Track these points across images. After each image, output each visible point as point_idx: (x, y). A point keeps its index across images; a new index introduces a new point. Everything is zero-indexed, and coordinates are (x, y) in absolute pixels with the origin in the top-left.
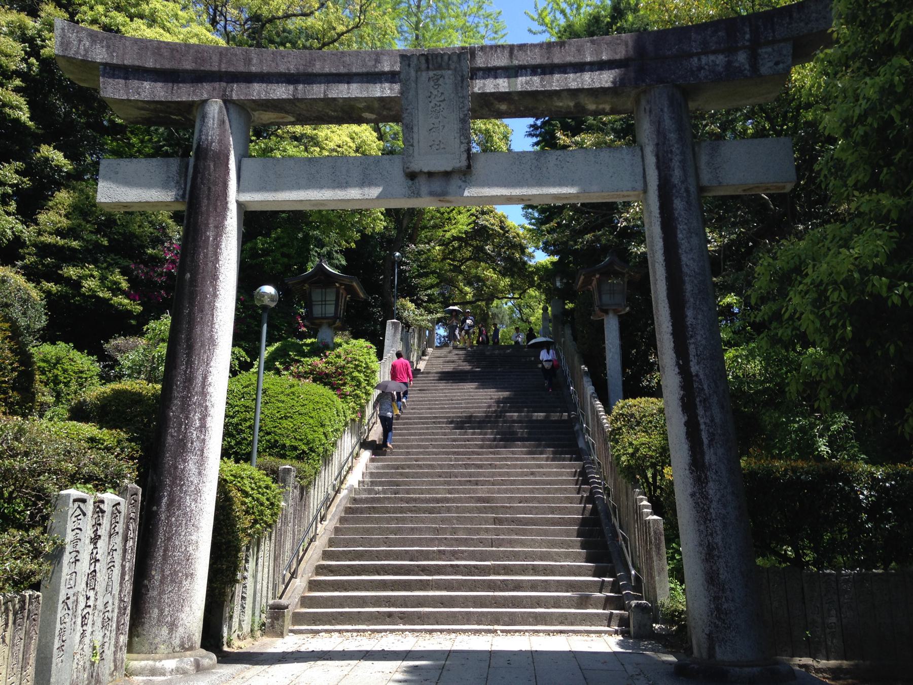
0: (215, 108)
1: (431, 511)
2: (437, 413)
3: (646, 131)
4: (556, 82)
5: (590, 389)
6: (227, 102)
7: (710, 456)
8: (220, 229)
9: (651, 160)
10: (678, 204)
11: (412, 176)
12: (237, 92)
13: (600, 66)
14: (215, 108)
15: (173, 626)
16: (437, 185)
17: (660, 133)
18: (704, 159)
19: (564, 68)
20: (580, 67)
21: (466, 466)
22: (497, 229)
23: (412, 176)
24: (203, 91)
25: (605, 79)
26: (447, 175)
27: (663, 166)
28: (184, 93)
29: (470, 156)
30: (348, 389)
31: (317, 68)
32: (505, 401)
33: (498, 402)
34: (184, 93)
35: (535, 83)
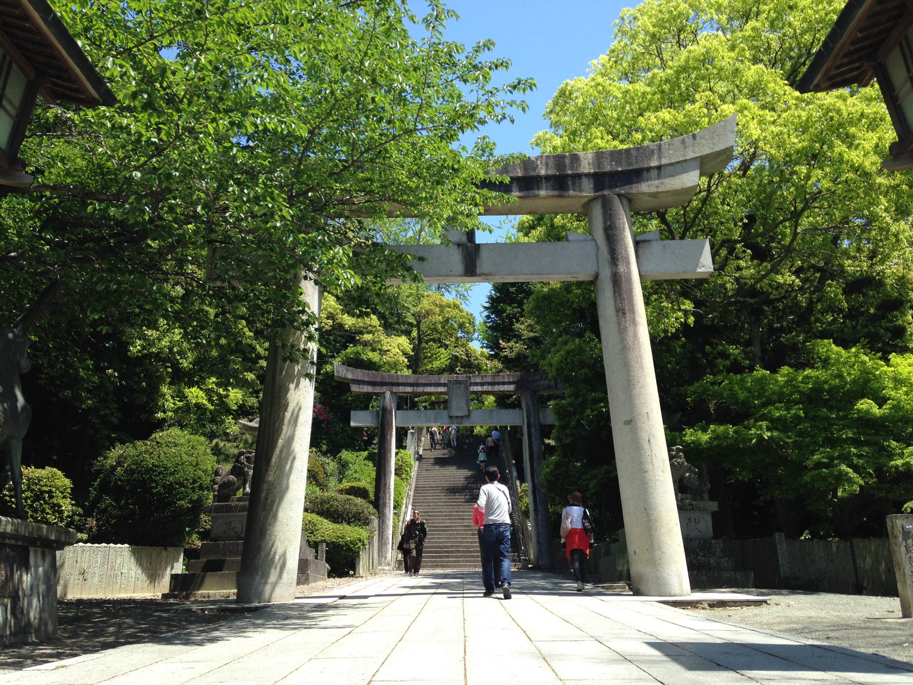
0: (388, 394)
1: (445, 531)
2: (438, 484)
3: (524, 405)
4: (497, 388)
5: (515, 474)
6: (392, 392)
7: (539, 508)
8: (391, 435)
9: (525, 415)
10: (533, 430)
11: (451, 417)
12: (395, 389)
13: (510, 383)
14: (388, 394)
15: (386, 558)
16: (459, 420)
17: (528, 406)
18: (541, 414)
19: (498, 383)
20: (504, 383)
21: (457, 512)
22: (464, 357)
23: (451, 417)
24: (384, 389)
25: (511, 388)
26: (462, 417)
27: (528, 417)
28: (378, 390)
29: (469, 411)
30: (404, 476)
31: (420, 381)
32: (471, 477)
33: (467, 478)
34: (378, 390)
35: (490, 388)
